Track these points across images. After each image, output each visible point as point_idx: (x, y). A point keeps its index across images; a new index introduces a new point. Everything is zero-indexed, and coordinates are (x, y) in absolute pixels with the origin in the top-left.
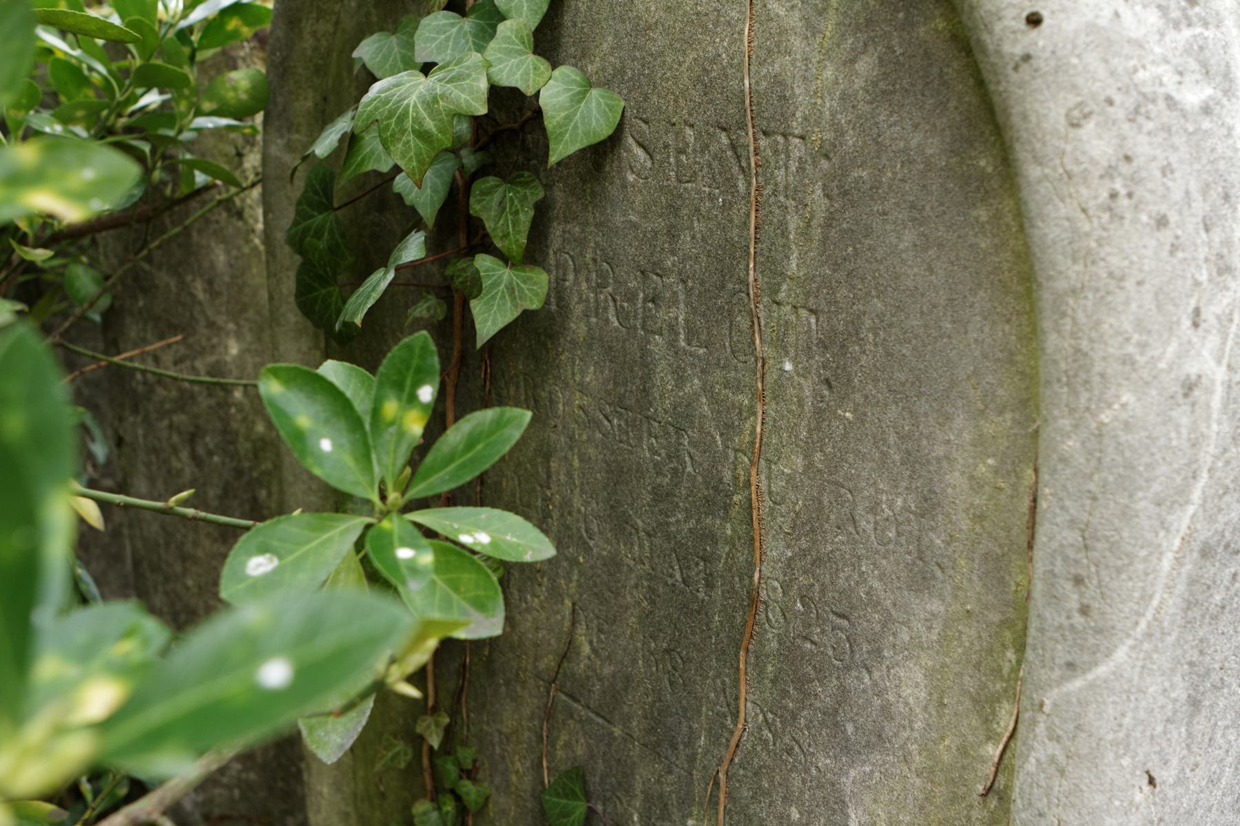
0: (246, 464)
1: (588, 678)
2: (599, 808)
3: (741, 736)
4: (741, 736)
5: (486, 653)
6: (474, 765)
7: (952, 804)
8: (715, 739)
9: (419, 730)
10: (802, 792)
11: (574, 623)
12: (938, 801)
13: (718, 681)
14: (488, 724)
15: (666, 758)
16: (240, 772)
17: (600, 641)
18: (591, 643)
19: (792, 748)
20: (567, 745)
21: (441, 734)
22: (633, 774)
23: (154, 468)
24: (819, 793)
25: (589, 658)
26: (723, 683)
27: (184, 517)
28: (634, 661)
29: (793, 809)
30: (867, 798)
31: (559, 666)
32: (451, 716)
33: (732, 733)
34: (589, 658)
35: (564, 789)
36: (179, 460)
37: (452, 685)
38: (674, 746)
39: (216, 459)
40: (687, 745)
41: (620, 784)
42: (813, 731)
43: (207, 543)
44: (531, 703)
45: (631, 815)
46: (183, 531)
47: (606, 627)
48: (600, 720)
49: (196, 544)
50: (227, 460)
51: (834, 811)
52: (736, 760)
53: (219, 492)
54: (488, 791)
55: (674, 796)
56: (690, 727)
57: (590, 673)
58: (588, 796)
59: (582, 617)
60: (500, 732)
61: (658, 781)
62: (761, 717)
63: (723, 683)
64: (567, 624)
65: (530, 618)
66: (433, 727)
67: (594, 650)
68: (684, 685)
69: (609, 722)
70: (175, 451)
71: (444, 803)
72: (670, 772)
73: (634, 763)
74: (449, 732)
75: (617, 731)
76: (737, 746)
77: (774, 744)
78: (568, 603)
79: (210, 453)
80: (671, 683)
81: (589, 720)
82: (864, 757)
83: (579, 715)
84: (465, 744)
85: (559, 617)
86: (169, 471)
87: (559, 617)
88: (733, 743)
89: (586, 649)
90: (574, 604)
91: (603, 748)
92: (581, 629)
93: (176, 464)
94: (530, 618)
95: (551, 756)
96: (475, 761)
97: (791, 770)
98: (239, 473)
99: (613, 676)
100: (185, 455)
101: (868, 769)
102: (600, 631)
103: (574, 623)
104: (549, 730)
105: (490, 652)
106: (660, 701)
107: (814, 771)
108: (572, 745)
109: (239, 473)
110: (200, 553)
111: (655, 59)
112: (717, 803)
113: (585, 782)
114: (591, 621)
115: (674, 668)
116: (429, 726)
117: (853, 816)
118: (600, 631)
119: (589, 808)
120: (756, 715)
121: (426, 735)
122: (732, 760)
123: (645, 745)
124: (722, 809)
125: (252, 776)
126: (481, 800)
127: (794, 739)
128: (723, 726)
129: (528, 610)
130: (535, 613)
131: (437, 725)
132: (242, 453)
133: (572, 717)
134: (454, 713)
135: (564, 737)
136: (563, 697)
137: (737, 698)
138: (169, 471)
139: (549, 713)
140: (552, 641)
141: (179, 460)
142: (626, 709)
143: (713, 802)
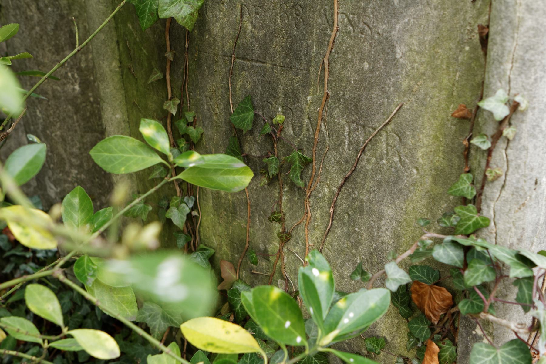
0: (65, 12)
1: (251, 43)
2: (261, 113)
3: (336, 35)
4: (336, 35)
5: (197, 56)
6: (194, 120)
7: (456, 16)
8: (321, 44)
9: (165, 108)
10: (370, 51)
11: (242, 17)
12: (447, 18)
13: (322, 11)
14: (200, 95)
15: (295, 68)
16: (77, 174)
17: (257, 19)
18: (252, 23)
19: (364, 29)
20: (243, 86)
21: (176, 108)
22: (278, 86)
23: (18, 17)
24: (379, 48)
25: (251, 32)
26: (325, 10)
27: (38, 137)
28: (276, 21)
29: (366, 63)
30: (406, 37)
31: (236, 44)
32: (180, 100)
33: (330, 36)
34: (251, 32)
35: (241, 110)
36: (31, 10)
37: (180, 83)
38: (299, 59)
39: (49, 9)
40: (305, 55)
41: (271, 95)
42: (375, 14)
43: (49, 55)
44: (221, 71)
45: (278, 109)
46: (37, 49)
47: (259, 9)
48: (259, 64)
49: (44, 56)
50: (55, 10)
51: (388, 53)
52: (333, 51)
53: (53, 27)
54: (202, 131)
55: (300, 87)
56: (308, 44)
57: (252, 40)
58: (254, 109)
59: (246, 10)
60: (206, 96)
61: (292, 83)
62: (346, 20)
63: (325, 10)
64: (239, 18)
65: (218, 24)
66: (172, 105)
67: (254, 26)
68: (303, 21)
69: (264, 63)
70: (28, 6)
71: (180, 143)
72: (298, 75)
73: (278, 79)
74: (180, 107)
75: (268, 66)
76: (334, 42)
77: (354, 31)
78: (239, 6)
79: (46, 6)
80: (296, 24)
81: (253, 67)
82: (404, 14)
83: (248, 67)
84: (189, 110)
85: (234, 16)
86: (26, 18)
87: (234, 16)
88: (332, 40)
89: (250, 27)
90: (241, 5)
91: (260, 79)
92: (246, 17)
93: (29, 13)
94: (218, 24)
95: (234, 96)
96: (194, 117)
97: (364, 42)
98: (62, 16)
99: (265, 35)
100: (33, 7)
101: (406, 20)
102: (257, 13)
103: (242, 17)
104: (231, 83)
105: (199, 54)
106: (291, 37)
107: (376, 36)
108: (244, 82)
109: (62, 16)
110: (46, 61)
111: (460, 23)
112: (324, 80)
113: (253, 103)
114: (252, 10)
115: (298, 15)
116: (170, 105)
117: (398, 51)
118: (257, 13)
119: (255, 114)
120: (344, 19)
121: (169, 109)
122: (331, 51)
123: (283, 66)
124: (326, 80)
125: (83, 176)
126: (199, 136)
127: (365, 23)
128: (326, 34)
129: (217, 21)
130: (221, 21)
131: (174, 104)
132: (63, 6)
133: (243, 69)
134: (182, 97)
135: (240, 83)
136: (238, 61)
137: (333, 15)
138: (26, 18)
139: (232, 74)
140: (231, 32)
141: (31, 10)
142: (272, 50)
143: (322, 80)
